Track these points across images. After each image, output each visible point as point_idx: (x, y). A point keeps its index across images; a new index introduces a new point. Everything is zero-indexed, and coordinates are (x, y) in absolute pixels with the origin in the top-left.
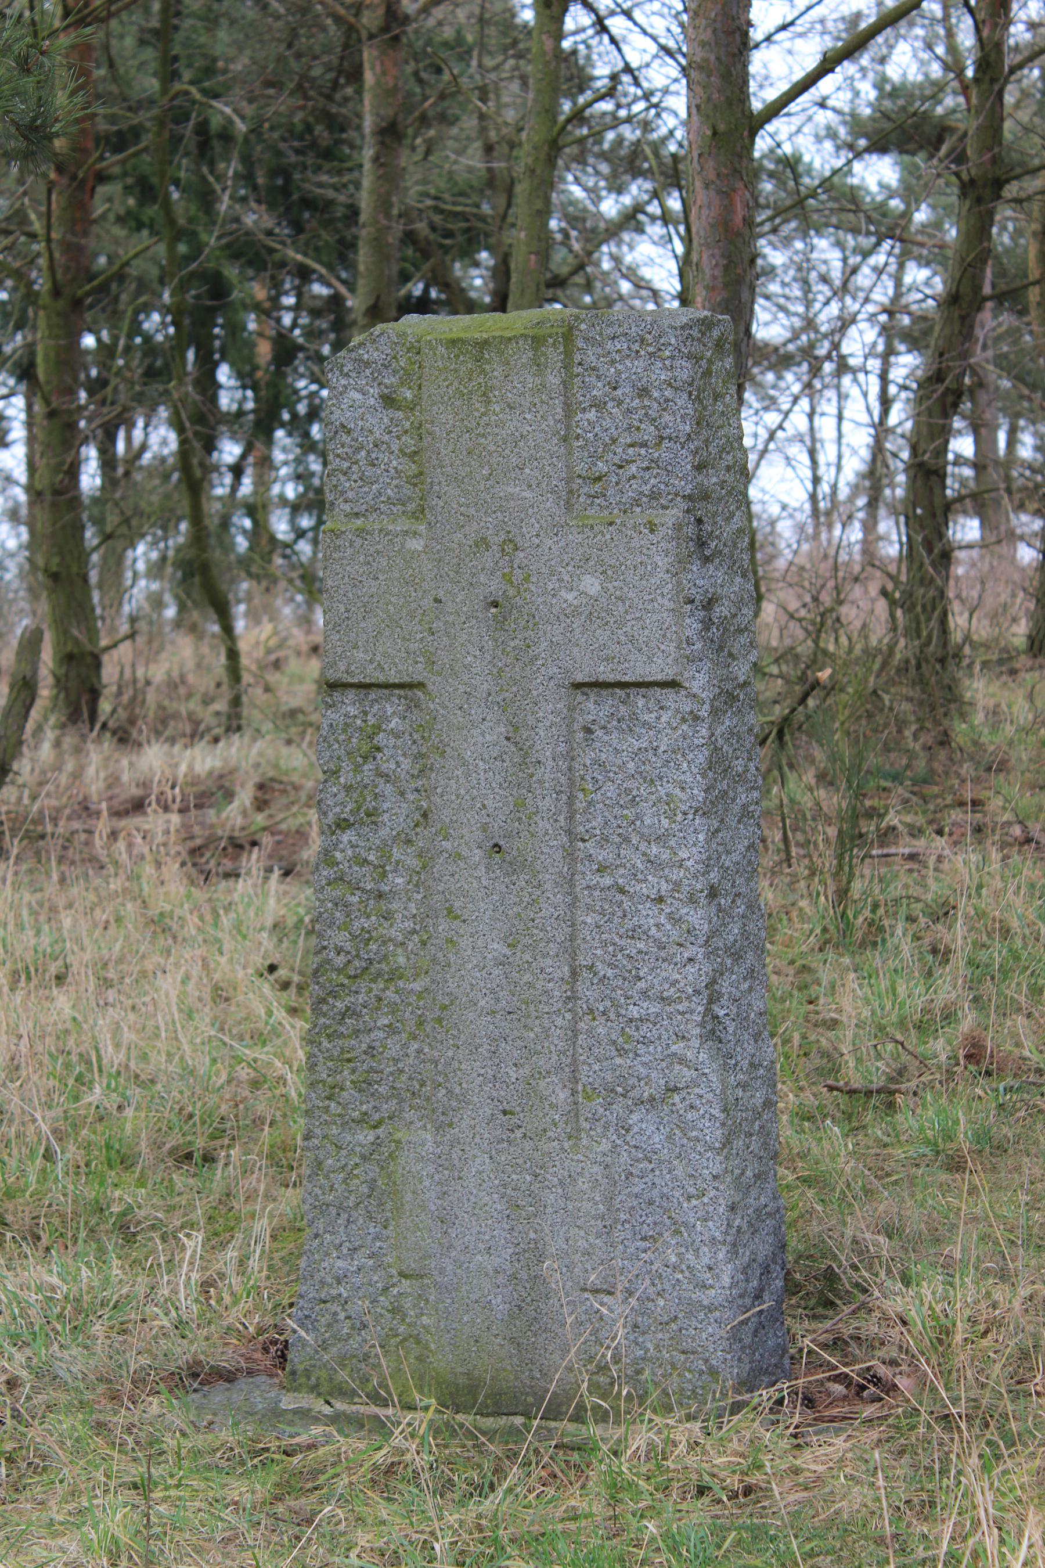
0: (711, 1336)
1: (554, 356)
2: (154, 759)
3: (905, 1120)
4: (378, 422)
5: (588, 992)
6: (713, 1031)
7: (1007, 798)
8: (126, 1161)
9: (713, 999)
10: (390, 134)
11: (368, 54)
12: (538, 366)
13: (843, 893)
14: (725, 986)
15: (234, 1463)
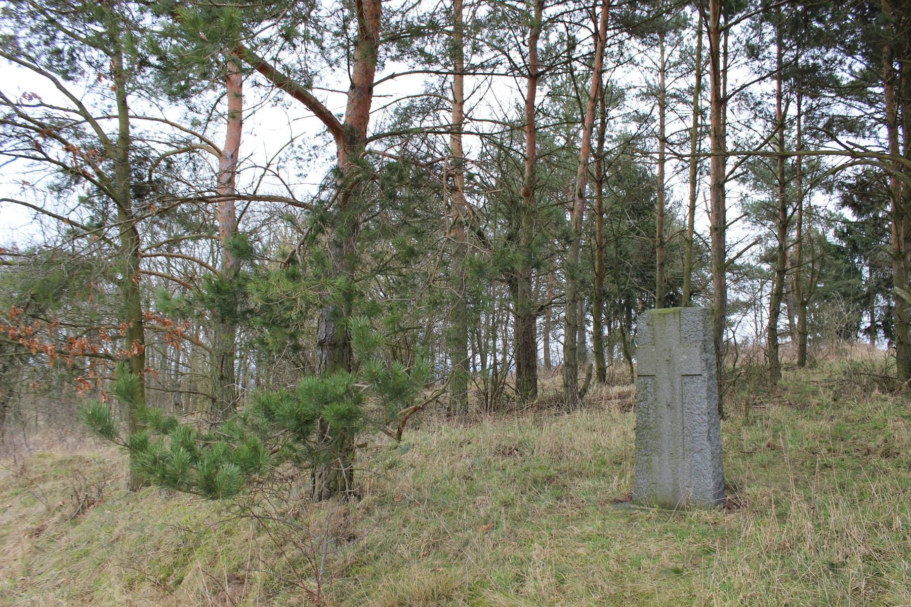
0: (709, 495)
1: (677, 316)
2: (617, 389)
3: (755, 458)
4: (646, 328)
5: (686, 431)
6: (709, 439)
7: (787, 396)
8: (605, 464)
9: (709, 433)
10: (662, 265)
11: (657, 250)
12: (674, 318)
13: (747, 415)
14: (711, 431)
15: (622, 516)
